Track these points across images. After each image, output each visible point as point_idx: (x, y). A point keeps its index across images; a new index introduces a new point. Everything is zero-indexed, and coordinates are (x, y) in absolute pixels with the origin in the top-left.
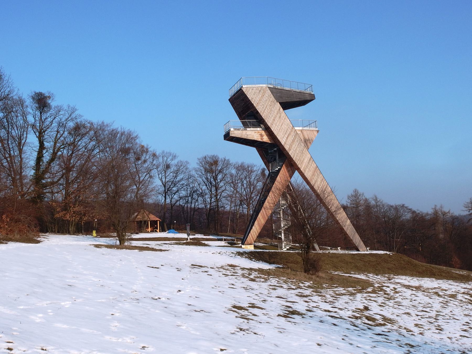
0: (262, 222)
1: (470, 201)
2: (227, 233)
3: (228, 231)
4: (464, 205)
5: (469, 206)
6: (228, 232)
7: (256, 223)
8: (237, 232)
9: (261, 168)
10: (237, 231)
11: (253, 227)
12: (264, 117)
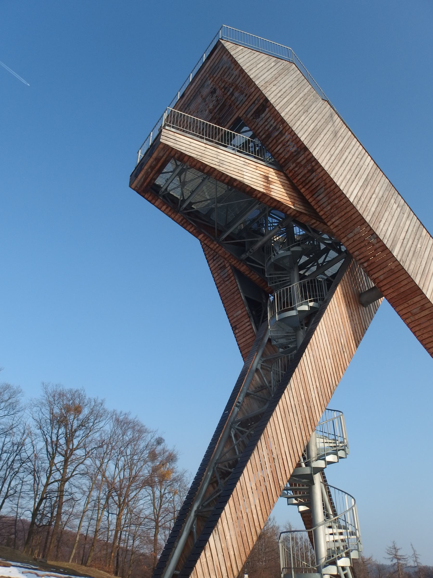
0: (255, 516)
1: (393, 545)
2: (68, 562)
3: (72, 557)
4: (386, 551)
5: (392, 552)
6: (71, 561)
7: (229, 516)
8: (89, 562)
9: (155, 438)
10: (90, 558)
11: (211, 539)
12: (287, 116)
